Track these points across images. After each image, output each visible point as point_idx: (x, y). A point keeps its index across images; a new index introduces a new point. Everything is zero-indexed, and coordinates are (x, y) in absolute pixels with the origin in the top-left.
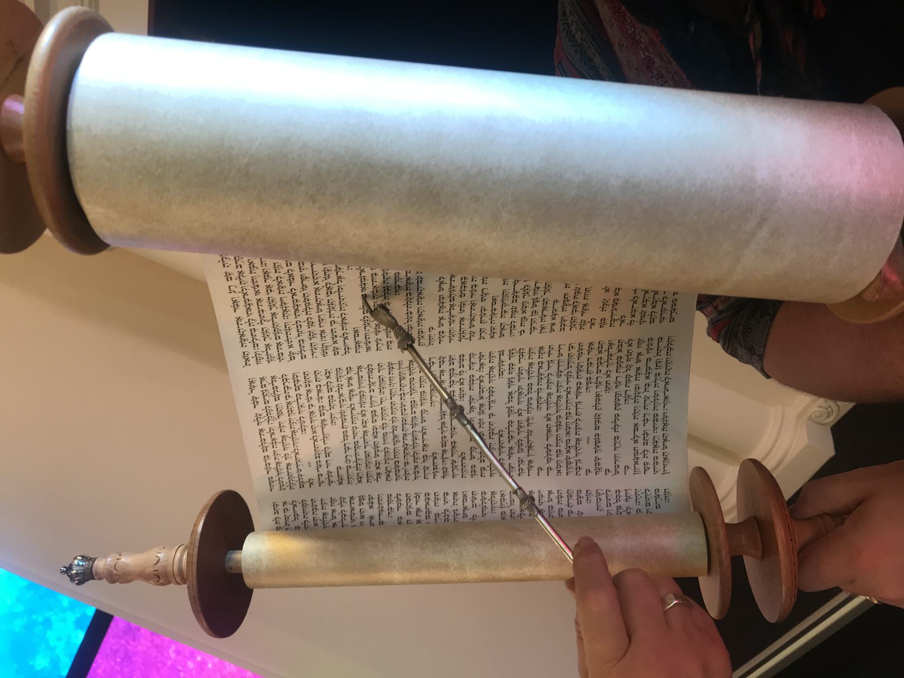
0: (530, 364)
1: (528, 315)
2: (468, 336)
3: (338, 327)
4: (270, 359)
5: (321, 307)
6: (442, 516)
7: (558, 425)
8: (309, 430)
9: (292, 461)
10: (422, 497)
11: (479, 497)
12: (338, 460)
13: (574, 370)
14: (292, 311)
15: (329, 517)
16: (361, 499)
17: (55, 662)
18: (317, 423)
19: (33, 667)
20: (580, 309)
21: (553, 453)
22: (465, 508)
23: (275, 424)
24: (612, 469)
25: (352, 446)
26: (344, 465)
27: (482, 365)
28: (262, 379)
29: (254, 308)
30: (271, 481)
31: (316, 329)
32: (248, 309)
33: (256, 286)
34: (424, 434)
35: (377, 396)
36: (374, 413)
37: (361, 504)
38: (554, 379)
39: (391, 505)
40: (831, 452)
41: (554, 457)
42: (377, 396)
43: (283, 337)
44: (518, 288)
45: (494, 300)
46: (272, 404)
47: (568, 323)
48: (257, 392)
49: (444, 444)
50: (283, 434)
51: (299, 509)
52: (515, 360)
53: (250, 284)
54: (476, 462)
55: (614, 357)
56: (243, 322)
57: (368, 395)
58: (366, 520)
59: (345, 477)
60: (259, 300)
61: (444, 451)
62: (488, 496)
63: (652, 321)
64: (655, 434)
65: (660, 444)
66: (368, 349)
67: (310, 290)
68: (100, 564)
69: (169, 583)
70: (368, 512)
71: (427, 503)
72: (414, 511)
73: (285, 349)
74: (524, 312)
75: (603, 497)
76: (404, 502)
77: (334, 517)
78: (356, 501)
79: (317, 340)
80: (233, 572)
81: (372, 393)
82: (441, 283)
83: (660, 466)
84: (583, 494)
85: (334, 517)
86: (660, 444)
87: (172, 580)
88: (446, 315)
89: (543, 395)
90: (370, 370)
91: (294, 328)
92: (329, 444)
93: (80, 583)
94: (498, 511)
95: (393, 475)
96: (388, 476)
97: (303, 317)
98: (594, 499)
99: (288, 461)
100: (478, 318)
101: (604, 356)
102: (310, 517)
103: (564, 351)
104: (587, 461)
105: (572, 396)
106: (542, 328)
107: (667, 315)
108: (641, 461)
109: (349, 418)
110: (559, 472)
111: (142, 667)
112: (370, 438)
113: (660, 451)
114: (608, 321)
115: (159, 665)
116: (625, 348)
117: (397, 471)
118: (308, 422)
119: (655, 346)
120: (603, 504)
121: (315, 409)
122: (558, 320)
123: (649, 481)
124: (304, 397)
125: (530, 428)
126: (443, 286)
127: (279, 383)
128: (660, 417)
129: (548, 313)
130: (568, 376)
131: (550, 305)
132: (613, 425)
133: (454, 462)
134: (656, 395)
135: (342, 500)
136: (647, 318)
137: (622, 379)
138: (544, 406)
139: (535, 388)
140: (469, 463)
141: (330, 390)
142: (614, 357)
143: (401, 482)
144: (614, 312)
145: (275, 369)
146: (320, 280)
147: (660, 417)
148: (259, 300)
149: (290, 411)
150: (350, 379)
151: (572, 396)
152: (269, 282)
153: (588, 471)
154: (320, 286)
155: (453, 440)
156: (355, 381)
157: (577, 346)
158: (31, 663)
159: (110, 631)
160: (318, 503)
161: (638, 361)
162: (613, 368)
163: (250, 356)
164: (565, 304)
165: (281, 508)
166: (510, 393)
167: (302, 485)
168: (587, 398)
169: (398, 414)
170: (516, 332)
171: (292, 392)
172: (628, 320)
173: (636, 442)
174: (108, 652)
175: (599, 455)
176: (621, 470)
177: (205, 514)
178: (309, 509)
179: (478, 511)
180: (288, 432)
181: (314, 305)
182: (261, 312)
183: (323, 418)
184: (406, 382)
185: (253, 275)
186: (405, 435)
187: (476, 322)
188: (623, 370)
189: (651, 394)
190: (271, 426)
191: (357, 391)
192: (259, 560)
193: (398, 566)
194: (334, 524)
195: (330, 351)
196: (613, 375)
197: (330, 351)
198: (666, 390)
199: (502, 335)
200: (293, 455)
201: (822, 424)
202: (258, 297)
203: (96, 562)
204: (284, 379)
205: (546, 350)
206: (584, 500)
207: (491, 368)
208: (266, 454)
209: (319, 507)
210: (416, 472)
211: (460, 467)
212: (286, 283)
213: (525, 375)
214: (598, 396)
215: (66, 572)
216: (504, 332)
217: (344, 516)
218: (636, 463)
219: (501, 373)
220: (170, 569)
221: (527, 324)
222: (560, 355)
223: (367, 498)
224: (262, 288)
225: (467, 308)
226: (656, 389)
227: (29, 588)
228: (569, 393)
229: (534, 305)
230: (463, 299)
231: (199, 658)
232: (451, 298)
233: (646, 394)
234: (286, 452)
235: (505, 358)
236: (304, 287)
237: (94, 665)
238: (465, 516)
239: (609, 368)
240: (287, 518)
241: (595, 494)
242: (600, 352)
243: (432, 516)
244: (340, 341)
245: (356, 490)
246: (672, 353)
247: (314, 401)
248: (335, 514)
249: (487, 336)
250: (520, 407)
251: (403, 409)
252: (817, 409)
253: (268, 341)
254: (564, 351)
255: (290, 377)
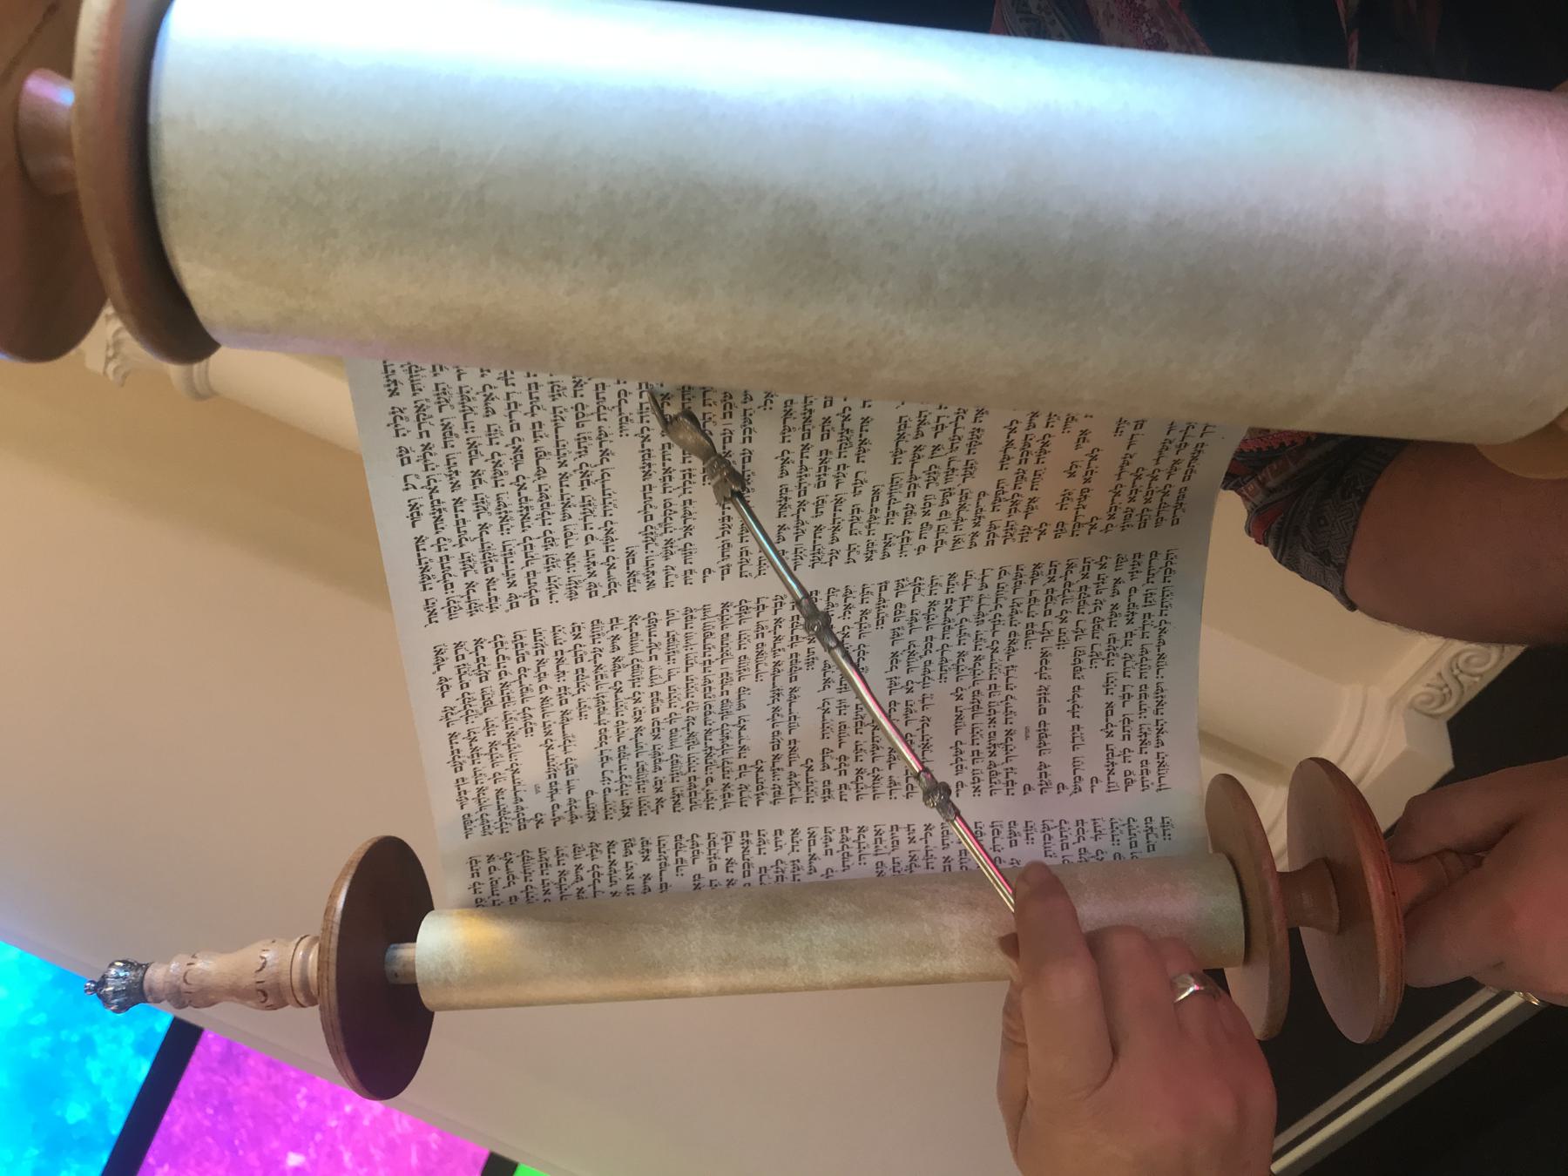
0: (932, 603)
1: (933, 519)
2: (826, 558)
3: (598, 547)
4: (473, 609)
5: (569, 511)
6: (772, 873)
7: (976, 708)
8: (539, 730)
9: (507, 785)
10: (737, 839)
11: (836, 836)
12: (588, 779)
13: (1005, 611)
14: (517, 518)
15: (571, 877)
16: (629, 844)
17: (100, 1113)
18: (555, 717)
19: (62, 1120)
20: (1022, 507)
21: (967, 756)
22: (813, 857)
23: (479, 723)
24: (1069, 783)
25: (614, 754)
26: (599, 788)
27: (848, 607)
28: (458, 645)
29: (449, 518)
30: (467, 821)
31: (559, 551)
32: (438, 519)
33: (452, 473)
34: (743, 728)
35: (662, 665)
36: (655, 696)
37: (628, 853)
38: (971, 628)
39: (681, 855)
40: (1448, 765)
41: (967, 763)
42: (662, 665)
43: (499, 567)
44: (918, 471)
45: (876, 493)
46: (475, 688)
47: (1000, 532)
48: (449, 669)
49: (776, 745)
50: (492, 739)
51: (516, 867)
52: (906, 597)
53: (443, 469)
54: (831, 775)
55: (1075, 588)
56: (427, 545)
57: (646, 665)
58: (638, 883)
59: (600, 808)
60: (458, 501)
61: (776, 757)
62: (853, 835)
63: (1143, 524)
64: (1142, 721)
65: (1152, 738)
66: (651, 584)
67: (552, 480)
68: (157, 975)
69: (284, 1004)
70: (640, 869)
71: (745, 850)
72: (721, 864)
73: (502, 590)
74: (926, 513)
75: (1055, 833)
76: (704, 849)
77: (579, 879)
78: (619, 849)
79: (560, 572)
80: (403, 981)
81: (654, 662)
82: (785, 461)
83: (1153, 778)
84: (1020, 828)
85: (579, 879)
86: (1152, 738)
87: (290, 999)
88: (790, 522)
89: (951, 655)
90: (652, 621)
91: (519, 551)
92: (574, 752)
93: (122, 1008)
94: (871, 861)
95: (685, 801)
96: (676, 803)
97: (536, 529)
98: (1038, 837)
99: (498, 786)
100: (846, 526)
101: (1059, 585)
102: (536, 879)
103: (992, 580)
104: (1026, 772)
105: (1001, 656)
106: (956, 541)
107: (1168, 514)
108: (1120, 768)
109: (610, 706)
110: (977, 789)
111: (250, 1123)
112: (646, 739)
113: (1151, 750)
114: (1069, 528)
115: (279, 1120)
116: (1095, 570)
117: (693, 793)
118: (537, 717)
119: (1144, 567)
120: (1056, 846)
121: (552, 693)
122: (983, 529)
123: (1133, 804)
124: (532, 673)
125: (926, 713)
126: (788, 467)
127: (488, 651)
128: (1151, 690)
129: (968, 515)
130: (996, 621)
131: (972, 502)
132: (1070, 705)
133: (792, 775)
134: (1144, 651)
135: (594, 847)
136: (1135, 520)
137: (1087, 626)
138: (952, 674)
139: (937, 644)
140: (818, 776)
141: (579, 658)
142: (1075, 588)
143: (701, 811)
144: (1081, 511)
145: (484, 625)
146: (569, 458)
147: (1151, 690)
148: (458, 501)
149: (506, 700)
150: (616, 638)
151: (1001, 656)
152: (479, 464)
153: (1027, 788)
154: (569, 469)
155: (792, 737)
156: (624, 643)
157: (1013, 571)
158: (59, 1113)
159: (194, 1059)
160: (551, 855)
161: (1116, 592)
162: (1072, 606)
163: (438, 607)
164: (997, 499)
165: (483, 867)
166: (895, 654)
167: (522, 826)
168: (1026, 660)
169: (698, 697)
170: (910, 549)
171: (511, 666)
172: (1101, 525)
173: (1110, 734)
174: (192, 1095)
175: (1046, 759)
176: (1085, 785)
177: (349, 878)
178: (535, 866)
179: (835, 862)
180: (501, 735)
181: (557, 507)
182: (460, 523)
183: (564, 708)
184: (715, 641)
185: (449, 450)
186: (708, 732)
187: (843, 535)
188: (1089, 608)
189: (1135, 650)
190: (470, 726)
191: (627, 660)
192: (448, 964)
193: (697, 960)
194: (580, 890)
195: (582, 590)
196: (1072, 618)
197: (582, 590)
198: (1161, 642)
199: (886, 555)
200: (509, 773)
201: (1431, 716)
202: (456, 495)
203: (149, 972)
204: (498, 642)
205: (961, 579)
206: (1021, 839)
207: (864, 612)
208: (459, 775)
209: (553, 861)
210: (726, 795)
211: (803, 785)
212: (508, 465)
213: (922, 622)
214: (1044, 654)
215: (95, 990)
216: (889, 550)
217: (596, 875)
218: (1111, 772)
219: (880, 621)
220: (284, 978)
221: (931, 535)
222: (984, 586)
223: (639, 843)
224: (465, 479)
225: (828, 509)
226: (1145, 641)
227: (56, 983)
228: (995, 650)
229: (945, 502)
230: (822, 491)
231: (348, 1109)
232: (802, 491)
233: (1127, 649)
234: (497, 769)
235: (889, 594)
236: (541, 472)
237: (167, 1118)
238: (813, 870)
239: (1065, 607)
240: (494, 884)
241: (1040, 828)
242: (1051, 580)
243: (755, 872)
244: (601, 570)
245: (618, 830)
246: (1172, 578)
247: (551, 680)
248: (581, 873)
249: (860, 558)
250: (911, 677)
251: (707, 688)
252: (1422, 689)
253: (471, 576)
254: (992, 580)
255: (509, 638)
